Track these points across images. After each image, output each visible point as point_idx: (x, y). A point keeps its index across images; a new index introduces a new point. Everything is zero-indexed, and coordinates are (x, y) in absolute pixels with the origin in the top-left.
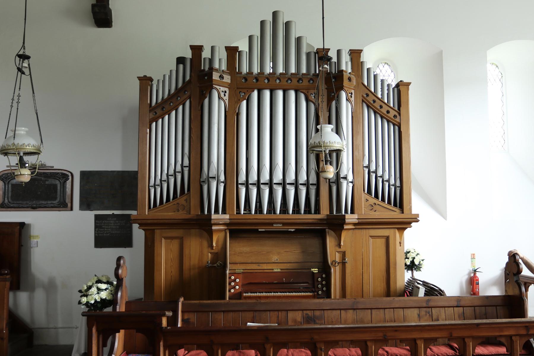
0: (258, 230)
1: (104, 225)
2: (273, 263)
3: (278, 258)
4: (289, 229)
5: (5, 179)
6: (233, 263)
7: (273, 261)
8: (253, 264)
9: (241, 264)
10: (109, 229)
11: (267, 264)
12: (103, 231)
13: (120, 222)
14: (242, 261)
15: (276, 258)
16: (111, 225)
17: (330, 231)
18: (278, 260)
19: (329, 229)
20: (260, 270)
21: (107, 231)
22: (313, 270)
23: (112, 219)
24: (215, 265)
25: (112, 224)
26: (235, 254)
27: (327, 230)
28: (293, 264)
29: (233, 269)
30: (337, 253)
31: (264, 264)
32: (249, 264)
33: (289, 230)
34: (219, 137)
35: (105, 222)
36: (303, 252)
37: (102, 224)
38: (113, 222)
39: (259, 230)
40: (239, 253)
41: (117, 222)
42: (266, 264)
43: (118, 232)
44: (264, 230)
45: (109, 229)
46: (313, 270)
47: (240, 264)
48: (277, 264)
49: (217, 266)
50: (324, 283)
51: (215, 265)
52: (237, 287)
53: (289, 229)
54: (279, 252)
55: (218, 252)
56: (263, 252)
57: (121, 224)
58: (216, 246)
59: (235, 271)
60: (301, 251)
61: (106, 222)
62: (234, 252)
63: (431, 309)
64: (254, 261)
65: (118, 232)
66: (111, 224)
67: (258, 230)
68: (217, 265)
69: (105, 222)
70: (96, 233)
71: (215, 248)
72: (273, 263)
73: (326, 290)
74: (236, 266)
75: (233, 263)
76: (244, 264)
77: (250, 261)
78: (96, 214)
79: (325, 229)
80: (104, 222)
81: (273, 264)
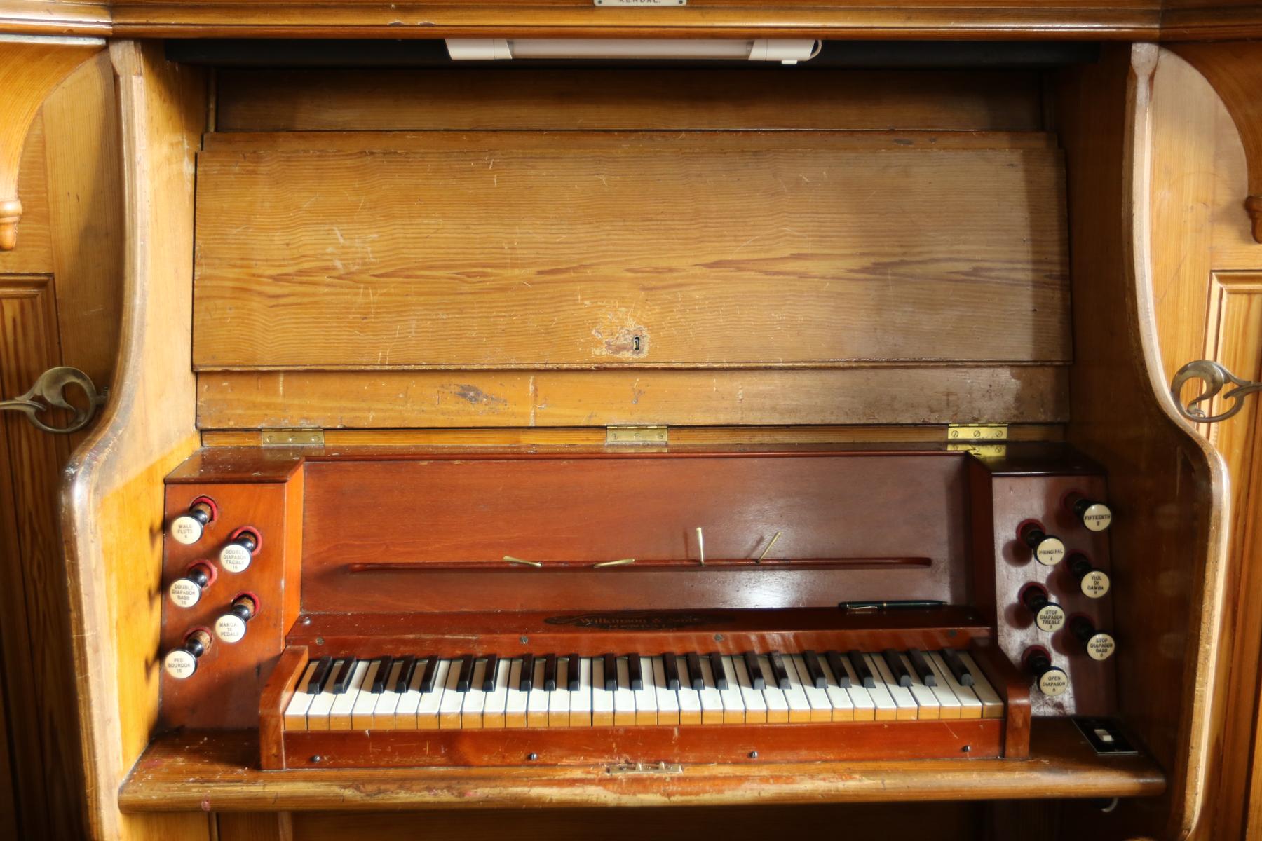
0: (437, 45)
2: (601, 370)
3: (646, 325)
4: (752, 37)
6: (226, 373)
7: (601, 353)
8: (413, 384)
9: (308, 382)
11: (544, 379)
14: (313, 358)
15: (631, 325)
17: (1171, 63)
18: (646, 345)
19: (1165, 43)
20: (486, 435)
22: (966, 433)
24: (22, 403)
26: (241, 291)
27: (1143, 54)
28: (789, 380)
29: (231, 424)
30: (1216, 285)
31: (518, 379)
32: (383, 383)
33: (760, 53)
34: (742, 373)
36: (876, 269)
39: (458, 52)
40: (277, 278)
42: (531, 379)
44: (499, 51)
46: (966, 433)
47: (295, 382)
48: (638, 381)
49: (39, 413)
50: (1096, 588)
51: (22, 403)
52: (231, 628)
53: (752, 37)
54: (657, 271)
55: (51, 275)
56: (504, 266)
58: (23, 217)
59: (252, 443)
60: (867, 262)
62: (232, 273)
63: (1196, 424)
64: (423, 356)
67: (437, 45)
68: (40, 399)
71: (20, 237)
72: (601, 370)
73: (1105, 663)
74: (260, 398)
75: (226, 373)
76: (333, 384)
77: (381, 356)
79: (1119, 48)
81: (603, 380)
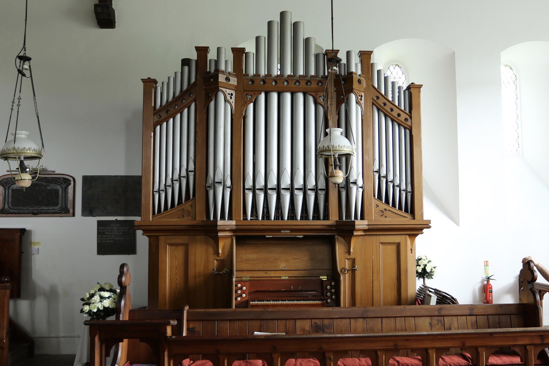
0: (265, 236)
1: (107, 232)
2: (281, 270)
4: (297, 235)
5: (5, 184)
6: (240, 271)
7: (281, 268)
8: (260, 272)
9: (248, 272)
10: (112, 236)
11: (275, 272)
12: (106, 237)
13: (123, 228)
14: (249, 269)
15: (284, 265)
16: (114, 232)
17: (339, 237)
18: (286, 267)
19: (338, 235)
20: (268, 278)
21: (110, 237)
22: (322, 277)
23: (115, 225)
25: (115, 231)
26: (241, 261)
27: (336, 236)
28: (302, 271)
29: (240, 276)
30: (346, 260)
31: (272, 271)
32: (256, 272)
33: (297, 236)
35: (108, 228)
36: (311, 259)
37: (105, 230)
38: (116, 228)
39: (267, 236)
40: (245, 260)
41: (121, 228)
42: (273, 271)
43: (122, 239)
44: (271, 236)
45: (112, 236)
46: (322, 277)
47: (247, 272)
48: (285, 271)
49: (223, 274)
50: (333, 291)
51: (221, 272)
52: (244, 295)
53: (297, 235)
54: (287, 259)
55: (224, 259)
56: (270, 259)
57: (125, 231)
58: (222, 253)
59: (241, 279)
60: (310, 258)
61: (109, 228)
62: (240, 260)
63: (443, 317)
64: (261, 269)
65: (122, 239)
66: (114, 231)
67: (265, 236)
68: (223, 272)
69: (108, 228)
70: (99, 240)
71: (221, 255)
72: (281, 270)
73: (335, 298)
74: (243, 274)
75: (240, 271)
76: (251, 272)
77: (257, 269)
78: (98, 221)
79: (334, 236)
80: (106, 228)
81: (281, 271)
